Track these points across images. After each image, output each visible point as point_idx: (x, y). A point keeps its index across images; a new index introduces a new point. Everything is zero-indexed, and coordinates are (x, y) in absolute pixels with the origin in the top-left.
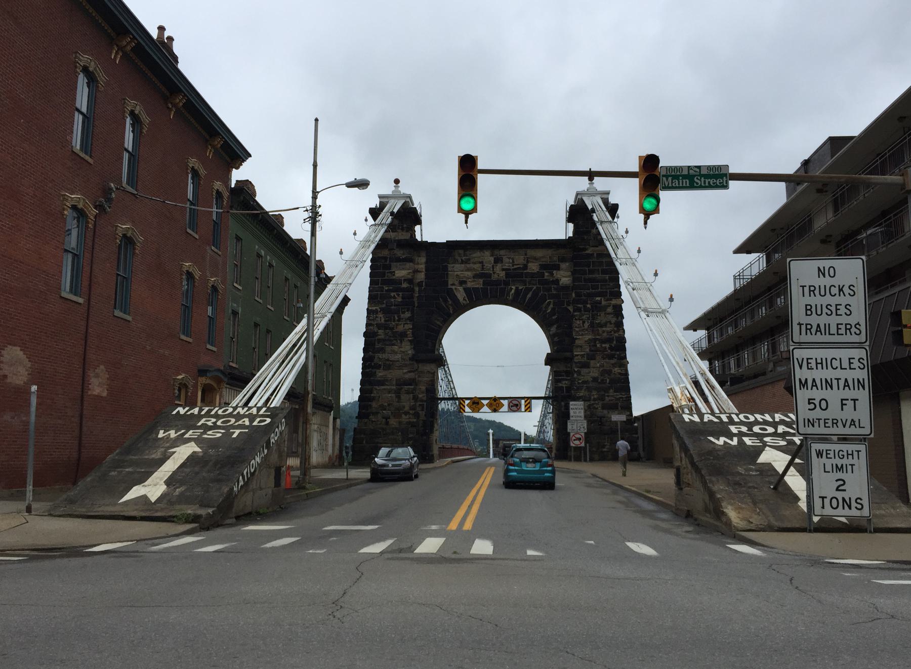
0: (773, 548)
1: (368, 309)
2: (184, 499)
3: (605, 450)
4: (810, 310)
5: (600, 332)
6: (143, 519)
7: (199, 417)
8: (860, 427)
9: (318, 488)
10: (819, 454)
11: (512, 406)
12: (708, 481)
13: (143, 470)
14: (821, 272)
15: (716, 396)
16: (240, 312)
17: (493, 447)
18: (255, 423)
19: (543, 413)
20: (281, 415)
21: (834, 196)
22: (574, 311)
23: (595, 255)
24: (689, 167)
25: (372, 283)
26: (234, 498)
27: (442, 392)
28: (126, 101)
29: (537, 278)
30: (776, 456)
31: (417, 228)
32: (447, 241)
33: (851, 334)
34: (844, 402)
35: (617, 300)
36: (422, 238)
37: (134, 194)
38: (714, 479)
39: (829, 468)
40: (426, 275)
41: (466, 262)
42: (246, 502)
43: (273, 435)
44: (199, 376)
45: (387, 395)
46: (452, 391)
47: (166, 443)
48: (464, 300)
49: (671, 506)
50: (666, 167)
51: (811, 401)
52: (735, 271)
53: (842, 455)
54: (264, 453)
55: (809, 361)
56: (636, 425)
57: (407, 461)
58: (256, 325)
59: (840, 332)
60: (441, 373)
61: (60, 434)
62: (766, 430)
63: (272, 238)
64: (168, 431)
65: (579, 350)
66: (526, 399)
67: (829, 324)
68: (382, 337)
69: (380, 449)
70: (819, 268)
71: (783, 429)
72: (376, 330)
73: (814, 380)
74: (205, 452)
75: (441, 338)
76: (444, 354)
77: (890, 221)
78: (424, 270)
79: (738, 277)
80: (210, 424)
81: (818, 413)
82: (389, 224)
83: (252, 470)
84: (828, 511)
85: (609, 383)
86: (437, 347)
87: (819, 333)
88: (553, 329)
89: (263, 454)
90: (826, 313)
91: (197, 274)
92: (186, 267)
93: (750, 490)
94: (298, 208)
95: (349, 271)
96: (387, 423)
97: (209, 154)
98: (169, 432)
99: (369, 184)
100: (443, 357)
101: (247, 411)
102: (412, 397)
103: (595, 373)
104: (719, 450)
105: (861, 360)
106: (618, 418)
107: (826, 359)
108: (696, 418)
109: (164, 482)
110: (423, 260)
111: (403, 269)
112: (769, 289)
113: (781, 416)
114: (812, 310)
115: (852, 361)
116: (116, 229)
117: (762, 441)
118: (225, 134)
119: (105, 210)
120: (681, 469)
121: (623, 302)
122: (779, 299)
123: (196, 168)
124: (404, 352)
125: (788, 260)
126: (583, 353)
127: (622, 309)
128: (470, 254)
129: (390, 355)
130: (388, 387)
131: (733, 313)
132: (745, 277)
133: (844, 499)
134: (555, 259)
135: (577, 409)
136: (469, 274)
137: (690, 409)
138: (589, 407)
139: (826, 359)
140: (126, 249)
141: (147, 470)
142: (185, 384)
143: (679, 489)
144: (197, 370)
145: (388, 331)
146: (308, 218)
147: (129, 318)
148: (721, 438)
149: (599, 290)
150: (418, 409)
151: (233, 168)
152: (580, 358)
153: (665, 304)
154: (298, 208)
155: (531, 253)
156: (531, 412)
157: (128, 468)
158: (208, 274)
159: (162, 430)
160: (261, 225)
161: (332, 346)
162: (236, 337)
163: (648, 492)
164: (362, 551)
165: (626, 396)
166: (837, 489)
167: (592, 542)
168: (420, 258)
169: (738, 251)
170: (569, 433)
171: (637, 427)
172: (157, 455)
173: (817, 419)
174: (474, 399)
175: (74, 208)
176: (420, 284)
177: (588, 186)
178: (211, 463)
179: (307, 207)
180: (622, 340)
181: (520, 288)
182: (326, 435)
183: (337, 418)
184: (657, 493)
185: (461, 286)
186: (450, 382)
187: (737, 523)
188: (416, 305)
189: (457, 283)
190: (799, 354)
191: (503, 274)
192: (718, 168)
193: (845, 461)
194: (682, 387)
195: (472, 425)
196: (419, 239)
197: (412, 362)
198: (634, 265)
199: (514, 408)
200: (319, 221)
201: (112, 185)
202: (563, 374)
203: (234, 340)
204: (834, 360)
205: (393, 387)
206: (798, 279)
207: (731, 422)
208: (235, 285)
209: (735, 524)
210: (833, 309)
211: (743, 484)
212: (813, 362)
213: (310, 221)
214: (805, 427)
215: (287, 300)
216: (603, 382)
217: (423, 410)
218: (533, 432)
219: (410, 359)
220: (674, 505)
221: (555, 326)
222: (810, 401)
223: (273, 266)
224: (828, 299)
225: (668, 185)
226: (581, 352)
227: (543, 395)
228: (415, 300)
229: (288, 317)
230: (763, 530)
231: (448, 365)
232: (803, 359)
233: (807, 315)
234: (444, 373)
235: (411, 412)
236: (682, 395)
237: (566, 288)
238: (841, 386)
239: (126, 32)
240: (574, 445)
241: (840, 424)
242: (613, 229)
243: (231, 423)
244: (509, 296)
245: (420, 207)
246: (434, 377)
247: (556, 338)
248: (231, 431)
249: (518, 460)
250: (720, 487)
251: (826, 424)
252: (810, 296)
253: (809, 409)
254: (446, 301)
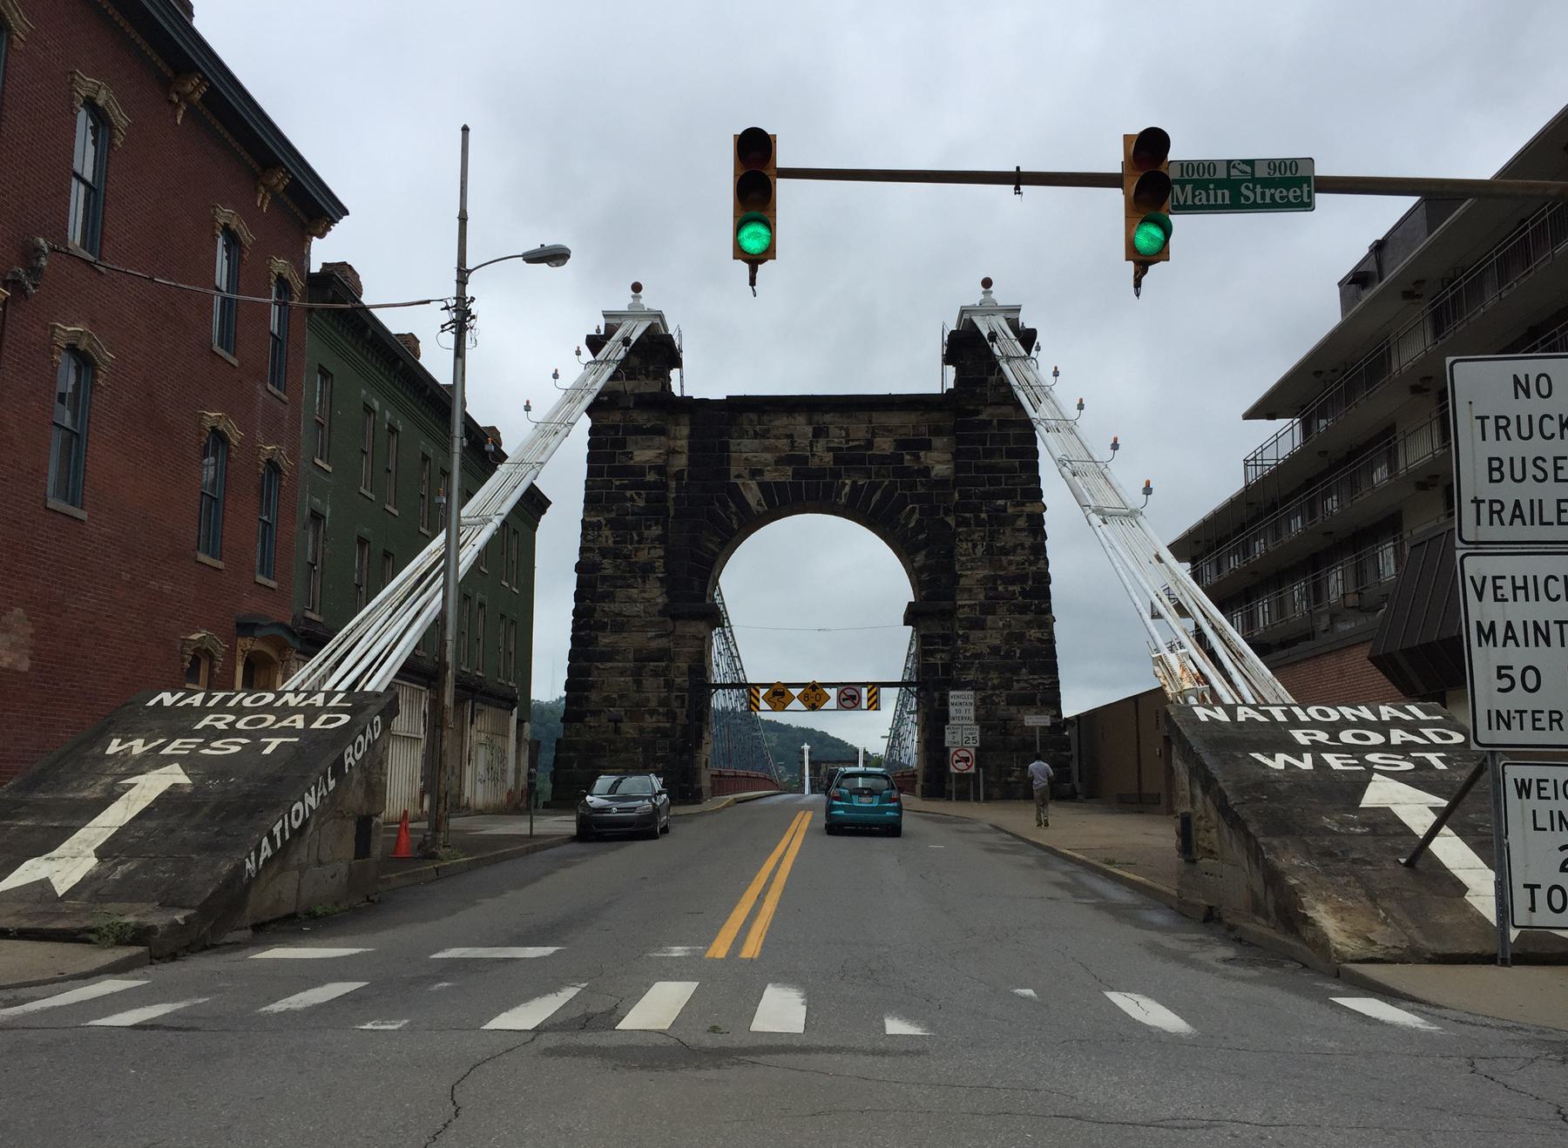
0: (1438, 1006)
1: (583, 521)
2: (128, 891)
3: (1012, 779)
4: (1499, 469)
5: (1005, 563)
6: (23, 935)
7: (203, 711)
9: (463, 857)
10: (1523, 789)
11: (844, 700)
12: (1264, 848)
13: (56, 824)
14: (1521, 386)
15: (1246, 672)
16: (328, 516)
17: (810, 775)
18: (316, 725)
19: (898, 713)
20: (372, 709)
21: (1433, 305)
22: (958, 525)
23: (995, 422)
24: (1229, 162)
25: (591, 472)
26: (247, 888)
27: (719, 672)
28: (77, 77)
29: (890, 464)
30: (1398, 792)
31: (674, 374)
32: (727, 397)
35: (1035, 504)
36: (682, 391)
37: (87, 262)
38: (1276, 842)
39: (1543, 821)
40: (690, 458)
41: (763, 435)
42: (285, 891)
43: (350, 749)
44: (237, 635)
45: (618, 679)
46: (738, 674)
47: (120, 767)
48: (758, 505)
49: (1168, 895)
50: (1181, 163)
51: (1503, 672)
52: (1247, 451)
54: (327, 788)
55: (1499, 582)
56: (1067, 733)
57: (647, 802)
58: (362, 542)
60: (717, 643)
61: (38, 751)
62: (1367, 738)
63: (423, 403)
64: (131, 740)
65: (966, 596)
66: (870, 687)
67: (1540, 501)
68: (609, 572)
69: (597, 779)
70: (1515, 377)
71: (1402, 736)
72: (598, 559)
73: (1509, 625)
74: (198, 787)
75: (716, 575)
76: (724, 607)
77: (1554, 340)
78: (686, 451)
79: (1253, 462)
80: (221, 725)
81: (1520, 699)
82: (622, 360)
83: (296, 825)
84: (1543, 917)
85: (1019, 658)
86: (709, 591)
87: (1518, 521)
88: (920, 558)
89: (324, 790)
90: (1534, 477)
91: (235, 435)
92: (209, 419)
93: (1356, 867)
94: (428, 302)
95: (541, 442)
96: (617, 731)
97: (262, 202)
98: (130, 743)
99: (569, 257)
100: (721, 612)
101: (304, 700)
102: (663, 683)
103: (996, 638)
104: (1278, 781)
106: (1036, 720)
107: (1535, 577)
108: (1221, 715)
109: (95, 851)
110: (685, 431)
111: (649, 447)
112: (1310, 483)
113: (1392, 710)
116: (53, 332)
117: (1362, 761)
118: (210, 71)
119: (24, 291)
120: (1194, 820)
121: (1045, 508)
122: (1257, 543)
123: (233, 227)
124: (648, 600)
125: (1449, 360)
126: (973, 602)
127: (1043, 522)
128: (771, 421)
129: (623, 605)
130: (620, 665)
131: (1243, 527)
132: (1265, 462)
134: (924, 429)
135: (962, 705)
136: (768, 457)
137: (1200, 698)
138: (983, 700)
139: (1535, 577)
140: (270, 479)
141: (66, 823)
142: (207, 650)
143: (1187, 861)
144: (235, 624)
145: (620, 560)
146: (450, 323)
147: (82, 515)
148: (1277, 755)
149: (1003, 486)
150: (675, 704)
151: (312, 235)
152: (968, 611)
153: (1135, 498)
154: (428, 302)
155: (881, 418)
156: (879, 710)
157: (24, 819)
158: (259, 436)
159: (117, 738)
160: (380, 358)
161: (517, 588)
162: (319, 564)
163: (1111, 863)
164: (495, 1024)
165: (1050, 680)
167: (1029, 992)
168: (678, 428)
169: (1251, 415)
170: (948, 749)
171: (1068, 738)
172: (93, 792)
173: (1516, 712)
174: (775, 687)
175: (72, 349)
176: (678, 476)
177: (982, 297)
178: (206, 810)
179: (448, 301)
180: (1044, 579)
181: (860, 483)
182: (504, 751)
183: (524, 722)
184: (1128, 865)
185: (754, 479)
186: (734, 657)
187: (1341, 944)
188: (672, 513)
189: (746, 473)
190: (1476, 567)
191: (829, 457)
192: (1291, 164)
194: (1183, 654)
195: (774, 737)
196: (677, 393)
197: (664, 619)
198: (1072, 431)
199: (849, 703)
200: (472, 328)
201: (42, 241)
202: (937, 640)
203: (316, 568)
205: (628, 665)
206: (1470, 403)
207: (1294, 722)
208: (318, 461)
209: (1338, 947)
210: (1549, 467)
211: (1340, 854)
212: (1506, 585)
213: (454, 330)
214: (1490, 728)
215: (427, 498)
216: (1009, 655)
217: (684, 707)
218: (879, 747)
219: (661, 613)
220: (1174, 893)
221: (924, 552)
223: (397, 431)
224: (1537, 446)
225: (1186, 201)
226: (970, 599)
228: (670, 504)
229: (486, 567)
230: (1401, 960)
231: (730, 626)
232: (1484, 578)
233: (1491, 481)
234: (724, 641)
235: (661, 710)
236: (1184, 670)
237: (942, 483)
239: (192, 69)
240: (956, 771)
242: (1029, 368)
243: (265, 725)
244: (841, 499)
245: (680, 335)
246: (704, 647)
247: (926, 575)
248: (263, 740)
249: (846, 791)
250: (1292, 862)
252: (1498, 439)
253: (1500, 690)
254: (726, 507)
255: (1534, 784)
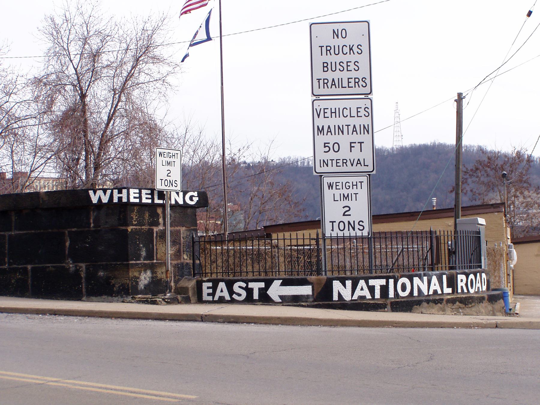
4: (326, 67)
8: (364, 165)
10: (330, 186)
33: (359, 87)
34: (352, 145)
51: (326, 145)
53: (348, 186)
59: (350, 85)
67: (342, 79)
73: (329, 127)
81: (332, 155)
105: (366, 109)
107: (339, 108)
114: (328, 67)
115: (359, 110)
133: (349, 223)
166: (344, 215)
193: (350, 191)
204: (344, 47)
210: (345, 65)
222: (325, 145)
224: (341, 58)
227: (466, 141)
233: (324, 71)
238: (350, 132)
241: (349, 163)
251: (338, 164)
253: (325, 152)
255: (322, 110)
